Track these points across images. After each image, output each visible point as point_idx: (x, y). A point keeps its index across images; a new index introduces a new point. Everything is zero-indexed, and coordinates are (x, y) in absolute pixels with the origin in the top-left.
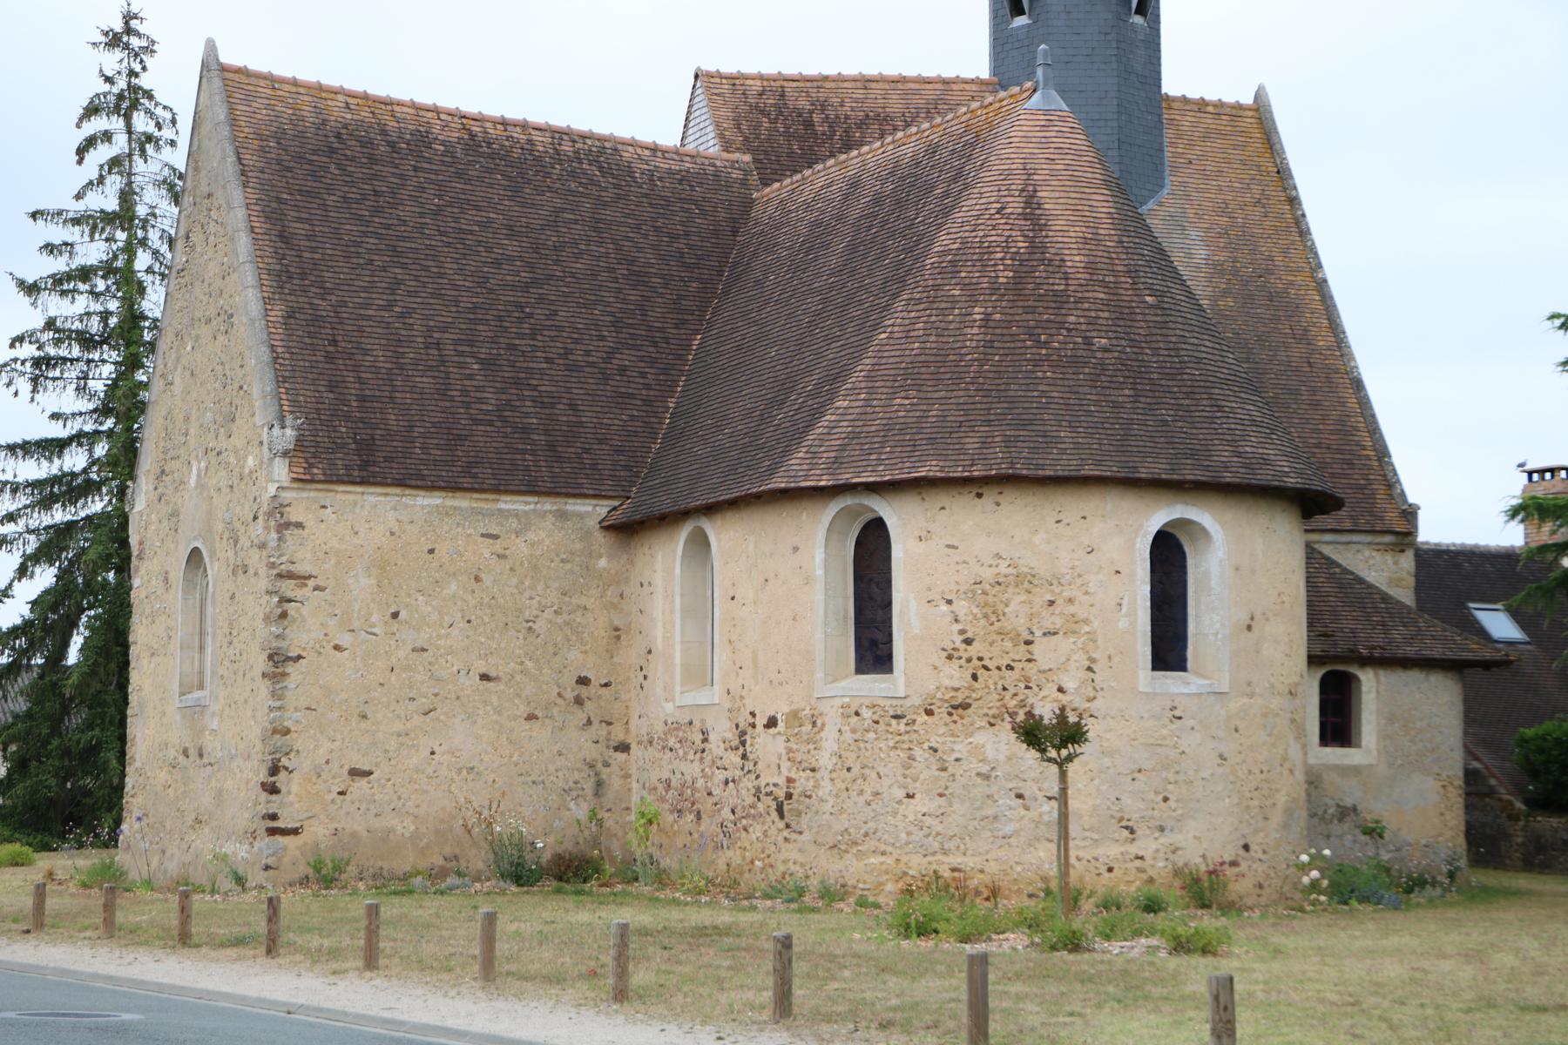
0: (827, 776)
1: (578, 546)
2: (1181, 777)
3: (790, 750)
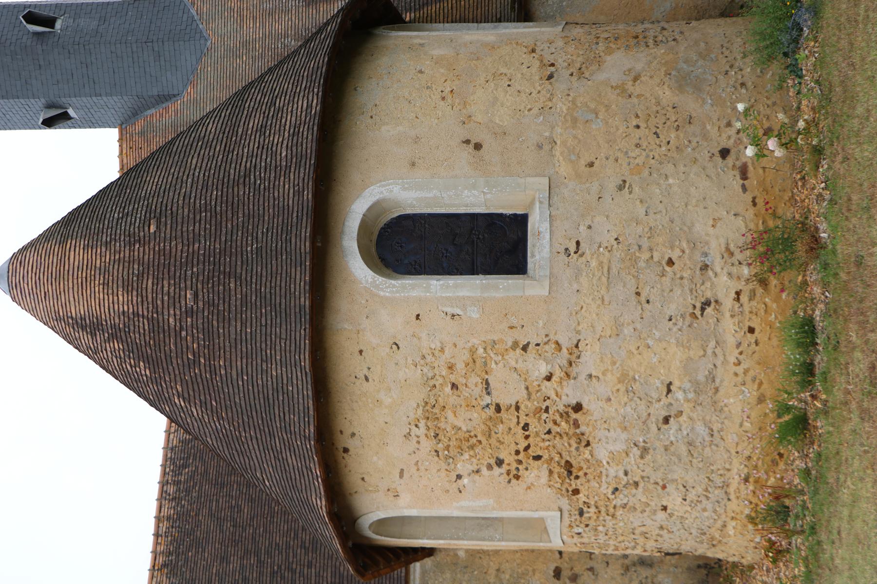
1: (448, 575)
2: (645, 243)
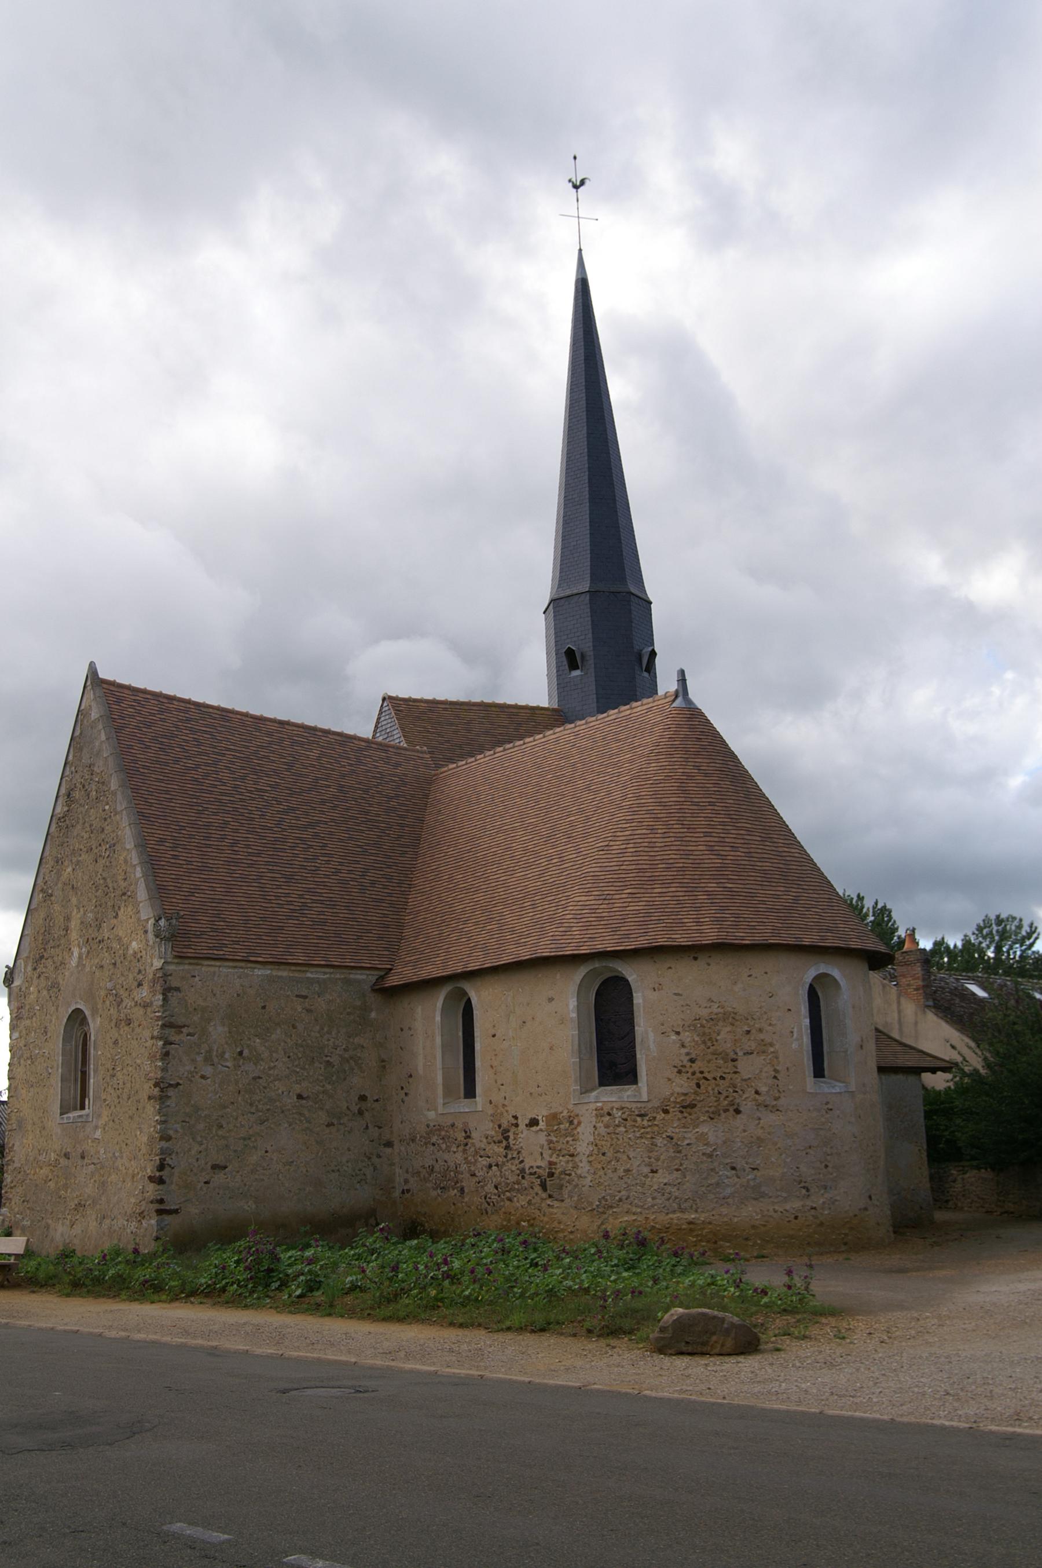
0: (585, 1159)
3: (550, 1142)
